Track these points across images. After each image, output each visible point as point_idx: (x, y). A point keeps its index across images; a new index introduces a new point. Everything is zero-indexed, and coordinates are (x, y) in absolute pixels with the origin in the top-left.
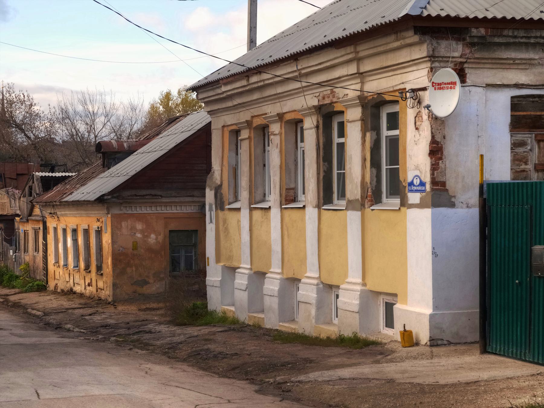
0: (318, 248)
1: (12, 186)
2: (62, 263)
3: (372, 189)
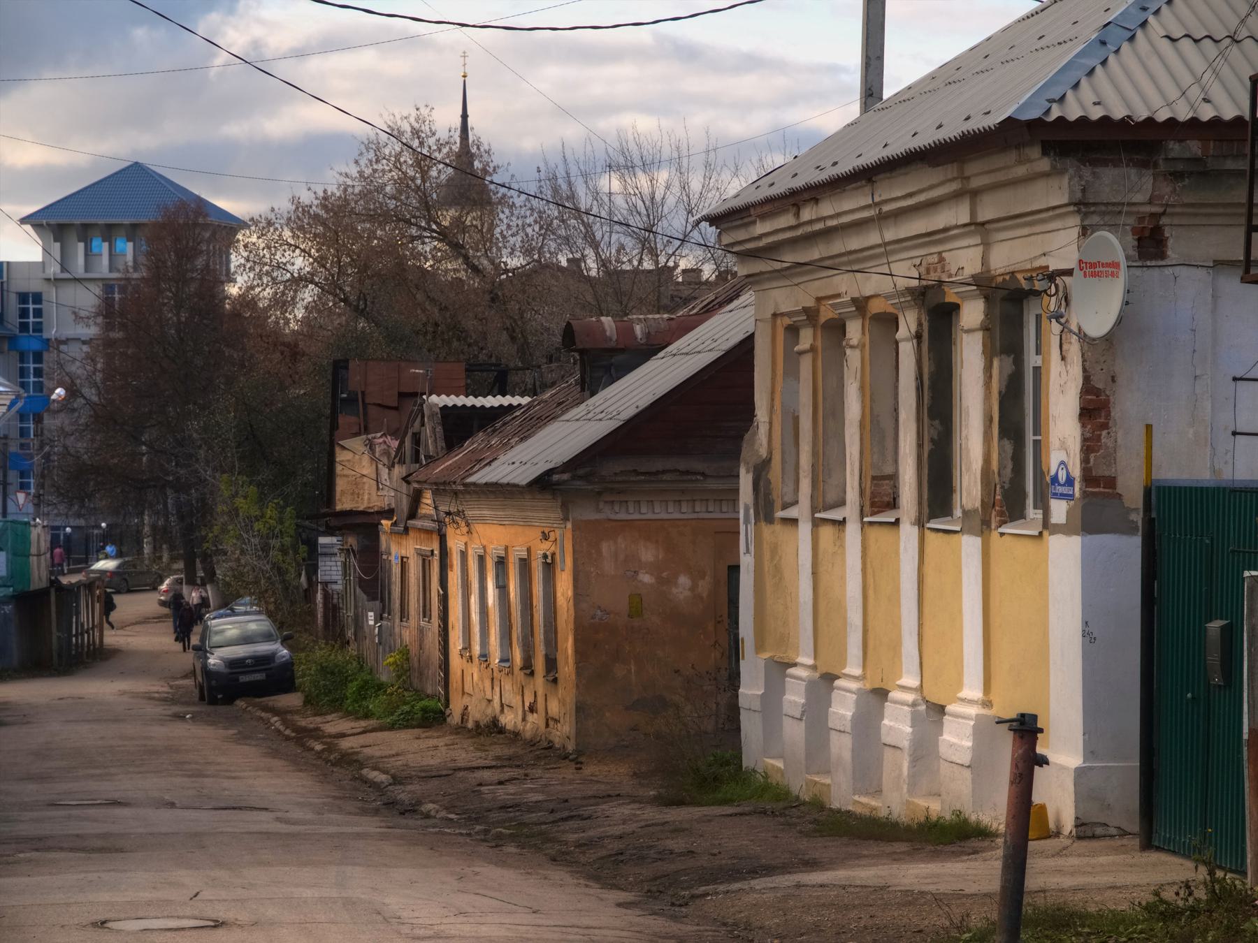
0: (919, 618)
1: (385, 428)
2: (477, 649)
3: (1002, 487)
